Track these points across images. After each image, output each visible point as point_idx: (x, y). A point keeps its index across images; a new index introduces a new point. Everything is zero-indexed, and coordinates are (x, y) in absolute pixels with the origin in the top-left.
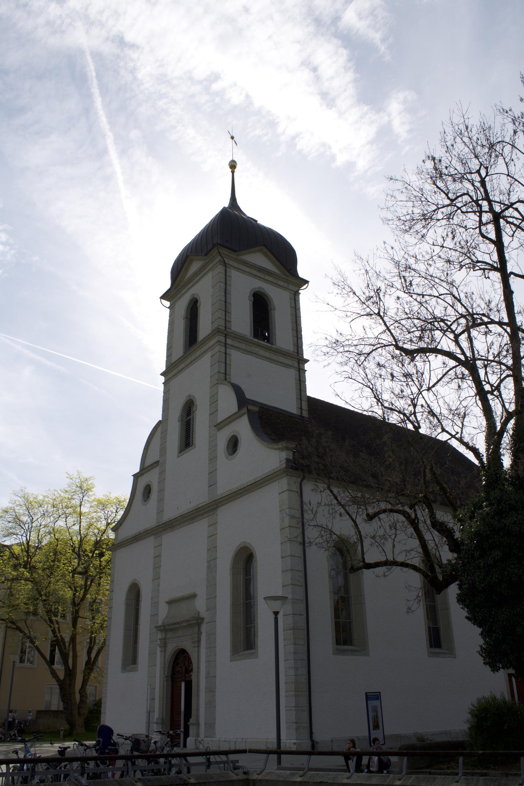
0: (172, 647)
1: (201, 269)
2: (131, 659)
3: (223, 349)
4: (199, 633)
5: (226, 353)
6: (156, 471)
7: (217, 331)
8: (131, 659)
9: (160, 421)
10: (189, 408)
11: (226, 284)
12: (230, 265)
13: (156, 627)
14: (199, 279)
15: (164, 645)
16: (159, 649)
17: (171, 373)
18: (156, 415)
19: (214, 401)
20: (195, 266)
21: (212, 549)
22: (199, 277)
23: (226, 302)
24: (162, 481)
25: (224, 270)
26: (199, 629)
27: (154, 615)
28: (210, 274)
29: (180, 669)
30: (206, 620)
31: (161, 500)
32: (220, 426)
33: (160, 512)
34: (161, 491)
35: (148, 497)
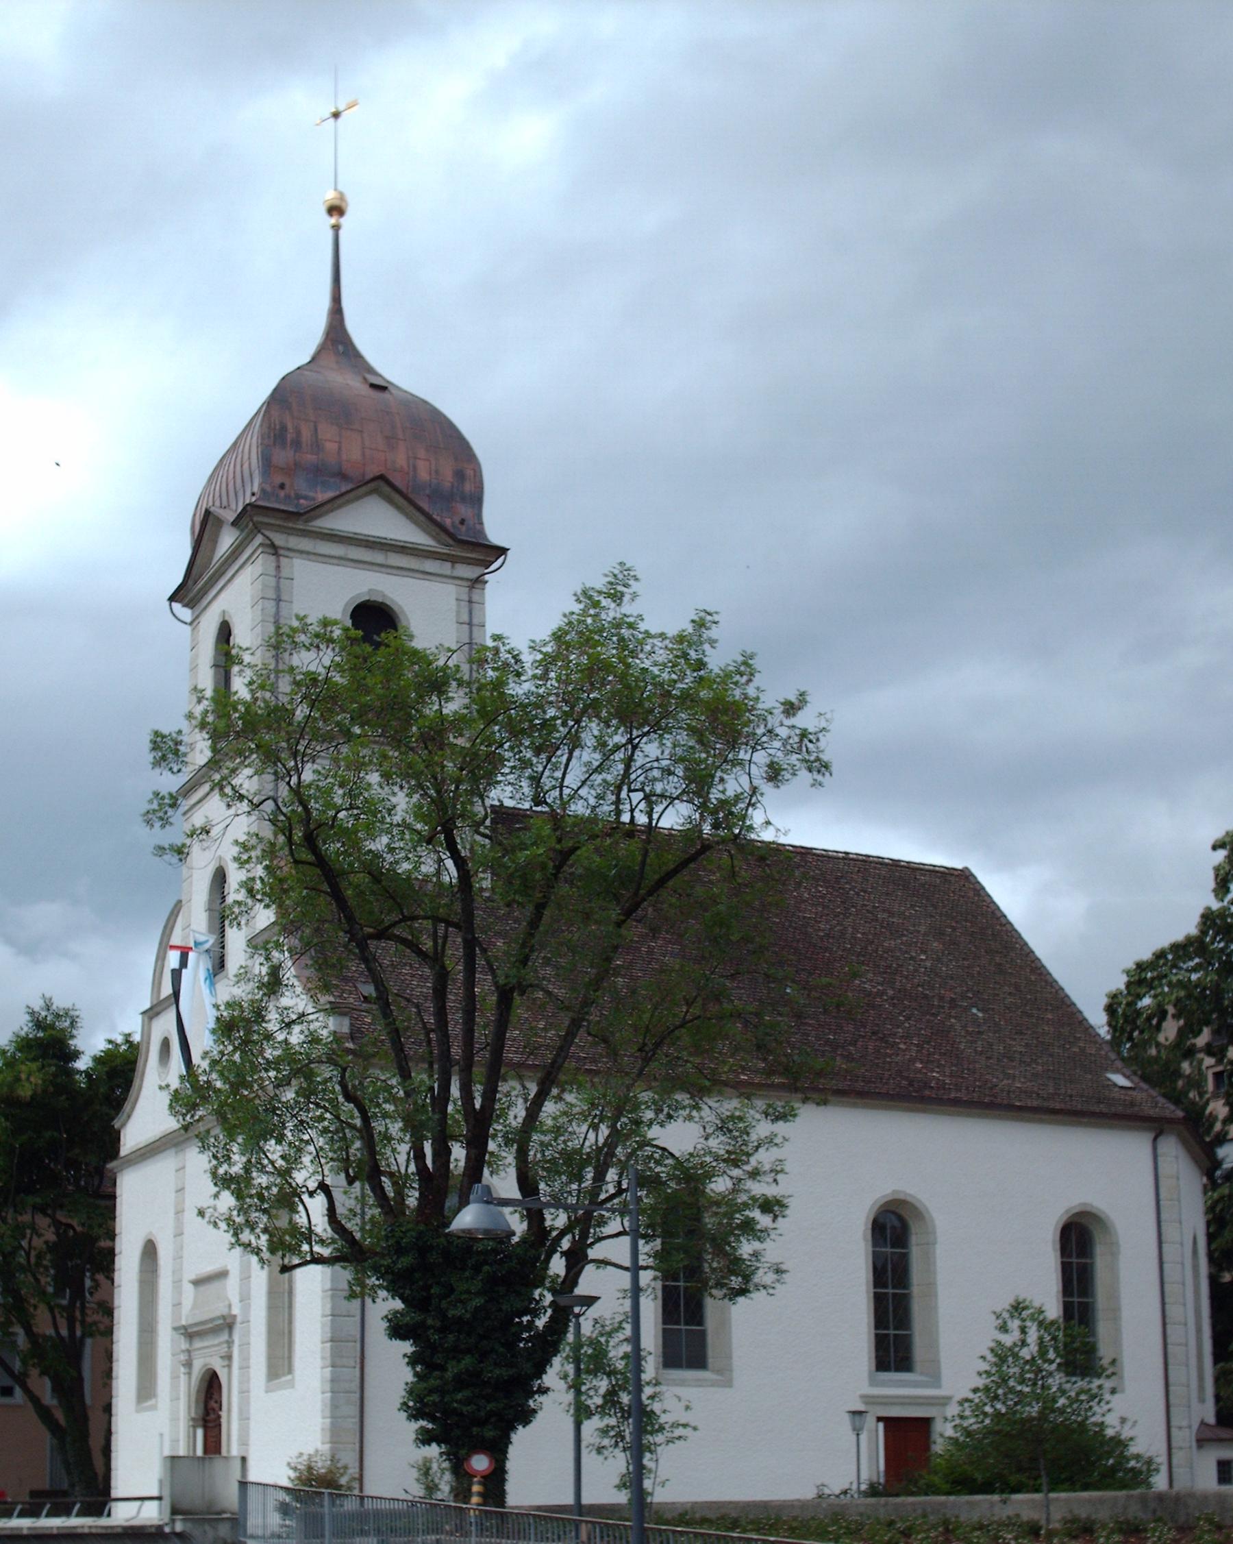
0: (198, 1366)
1: (235, 552)
2: (146, 1390)
4: (230, 1343)
8: (146, 1390)
14: (233, 576)
15: (188, 1364)
16: (182, 1369)
25: (274, 565)
27: (177, 1305)
29: (209, 1398)
30: (239, 1319)
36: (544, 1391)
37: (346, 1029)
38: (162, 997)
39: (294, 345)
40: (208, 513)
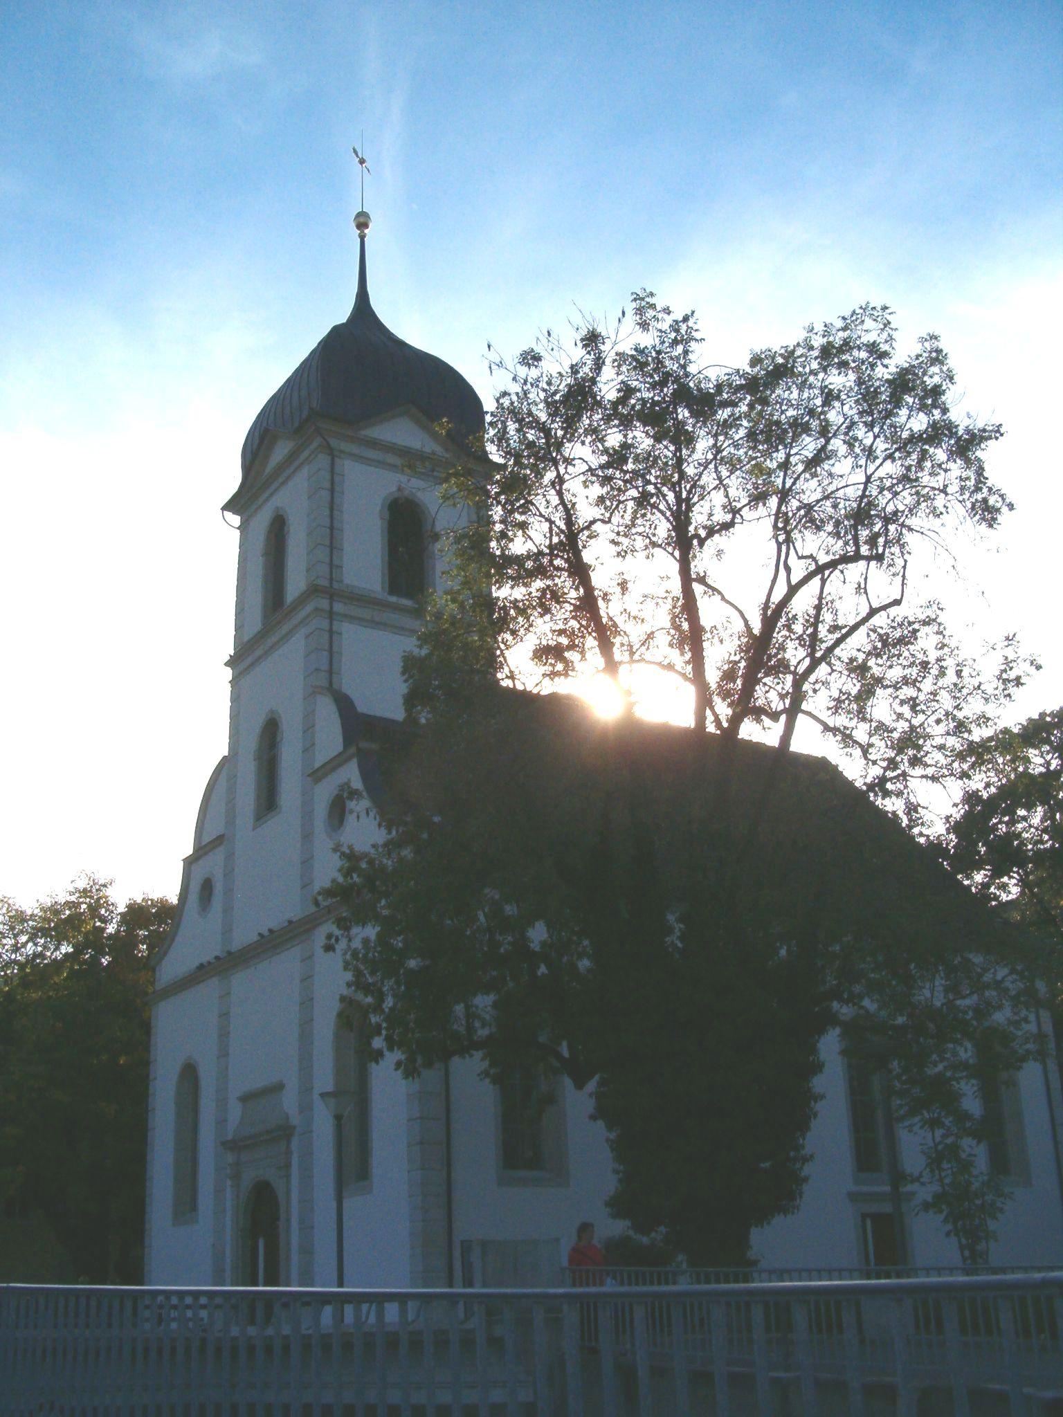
1: (293, 456)
2: (186, 1205)
3: (325, 624)
4: (288, 1152)
5: (331, 631)
6: (218, 856)
7: (313, 591)
8: (186, 1205)
9: (225, 757)
10: (271, 732)
11: (332, 491)
12: (342, 452)
13: (223, 1143)
16: (229, 1182)
17: (245, 659)
18: (221, 748)
19: (309, 728)
20: (281, 451)
21: (307, 1002)
22: (285, 474)
23: (332, 528)
24: (229, 874)
26: (288, 1147)
27: (222, 1122)
28: (305, 471)
29: (262, 1215)
31: (228, 910)
32: (317, 775)
33: (227, 931)
34: (229, 891)
35: (209, 900)
36: (471, 1056)
37: (854, 691)
38: (317, 765)
39: (342, 312)
40: (266, 431)
